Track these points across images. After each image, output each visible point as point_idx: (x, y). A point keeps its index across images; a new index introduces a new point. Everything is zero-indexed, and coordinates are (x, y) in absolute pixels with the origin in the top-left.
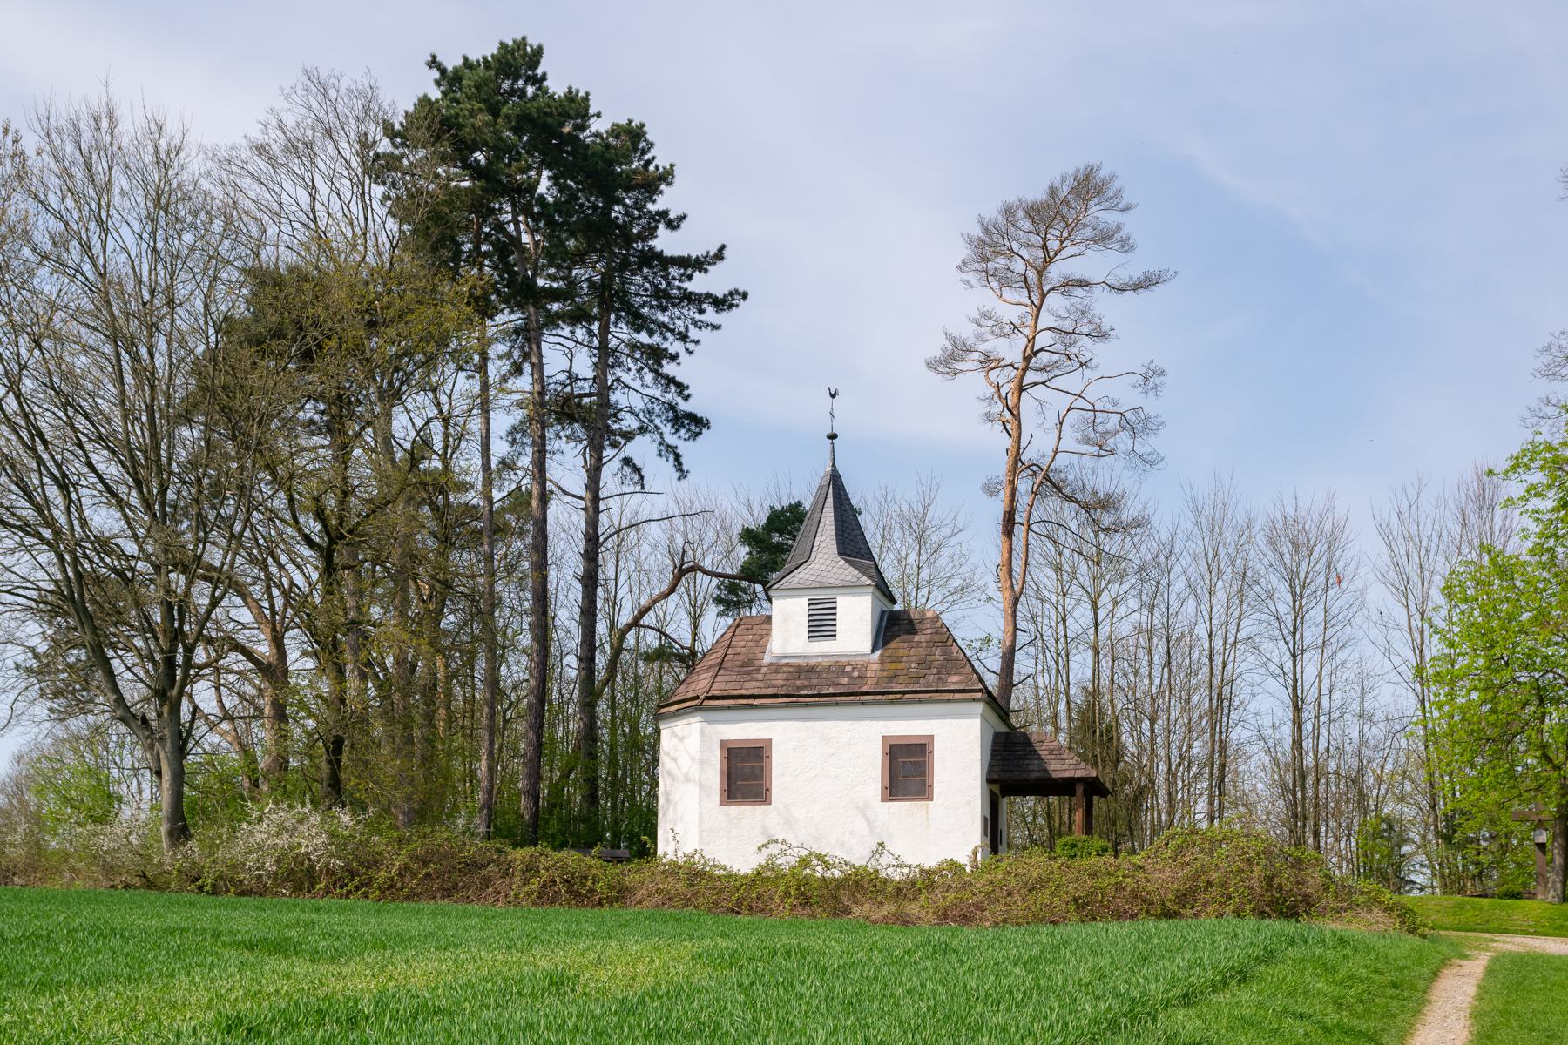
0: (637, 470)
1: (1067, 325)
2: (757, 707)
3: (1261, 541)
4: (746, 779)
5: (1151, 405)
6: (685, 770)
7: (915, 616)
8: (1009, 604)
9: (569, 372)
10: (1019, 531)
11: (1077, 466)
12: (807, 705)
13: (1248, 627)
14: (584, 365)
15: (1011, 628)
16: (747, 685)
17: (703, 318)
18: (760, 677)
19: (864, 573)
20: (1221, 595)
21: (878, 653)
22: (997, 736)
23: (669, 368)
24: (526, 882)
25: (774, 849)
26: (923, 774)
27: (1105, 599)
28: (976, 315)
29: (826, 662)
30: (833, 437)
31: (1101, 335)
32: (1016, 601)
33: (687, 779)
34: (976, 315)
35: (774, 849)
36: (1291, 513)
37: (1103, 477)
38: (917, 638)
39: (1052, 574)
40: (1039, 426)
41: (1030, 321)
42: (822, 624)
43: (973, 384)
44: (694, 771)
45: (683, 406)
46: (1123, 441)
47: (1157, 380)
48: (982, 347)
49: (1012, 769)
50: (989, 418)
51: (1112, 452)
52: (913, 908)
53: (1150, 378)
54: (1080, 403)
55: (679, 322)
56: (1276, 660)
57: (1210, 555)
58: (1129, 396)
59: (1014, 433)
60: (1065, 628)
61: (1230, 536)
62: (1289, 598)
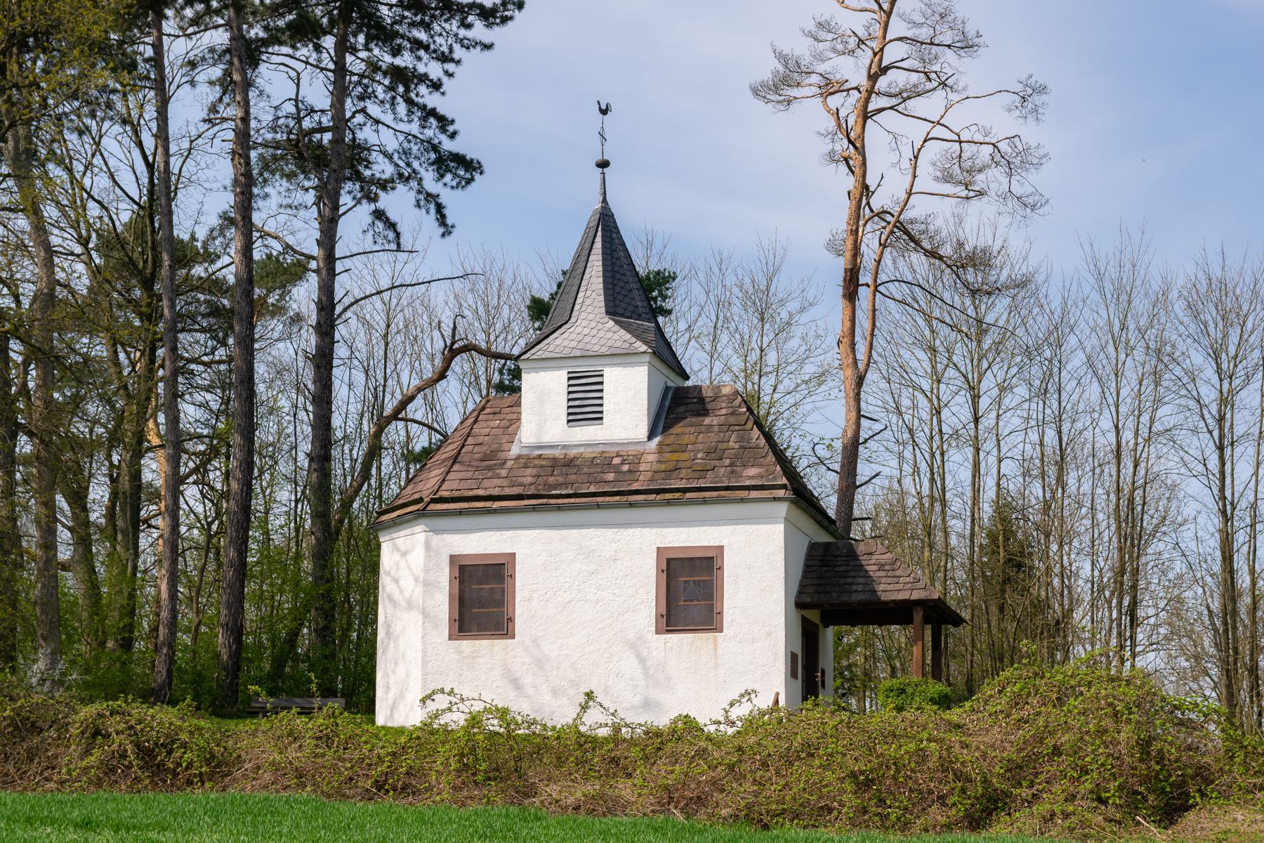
0: (392, 226)
1: (924, 34)
2: (495, 511)
3: (1179, 308)
4: (483, 606)
5: (1031, 133)
6: (407, 594)
7: (707, 393)
8: (850, 384)
9: (296, 100)
10: (864, 293)
11: (935, 211)
12: (559, 508)
13: (1167, 415)
14: (318, 92)
15: (854, 414)
16: (486, 483)
17: (469, 34)
18: (504, 473)
19: (638, 337)
20: (1131, 376)
21: (657, 440)
22: (813, 547)
23: (426, 96)
24: (87, 752)
25: (442, 702)
26: (711, 598)
27: (989, 384)
28: (811, 26)
29: (588, 453)
30: (603, 164)
31: (966, 45)
32: (860, 380)
33: (410, 605)
34: (811, 26)
35: (442, 702)
36: (1217, 272)
37: (978, 224)
38: (707, 421)
39: (923, 356)
40: (893, 165)
41: (877, 30)
42: (585, 404)
43: (811, 119)
44: (418, 593)
45: (448, 145)
46: (994, 179)
47: (1037, 99)
48: (821, 68)
49: (831, 592)
50: (832, 157)
51: (981, 194)
52: (625, 789)
53: (1028, 97)
54: (939, 132)
55: (439, 40)
56: (1198, 454)
57: (1116, 328)
58: (999, 120)
59: (857, 171)
60: (940, 422)
61: (1141, 305)
62: (1215, 379)
